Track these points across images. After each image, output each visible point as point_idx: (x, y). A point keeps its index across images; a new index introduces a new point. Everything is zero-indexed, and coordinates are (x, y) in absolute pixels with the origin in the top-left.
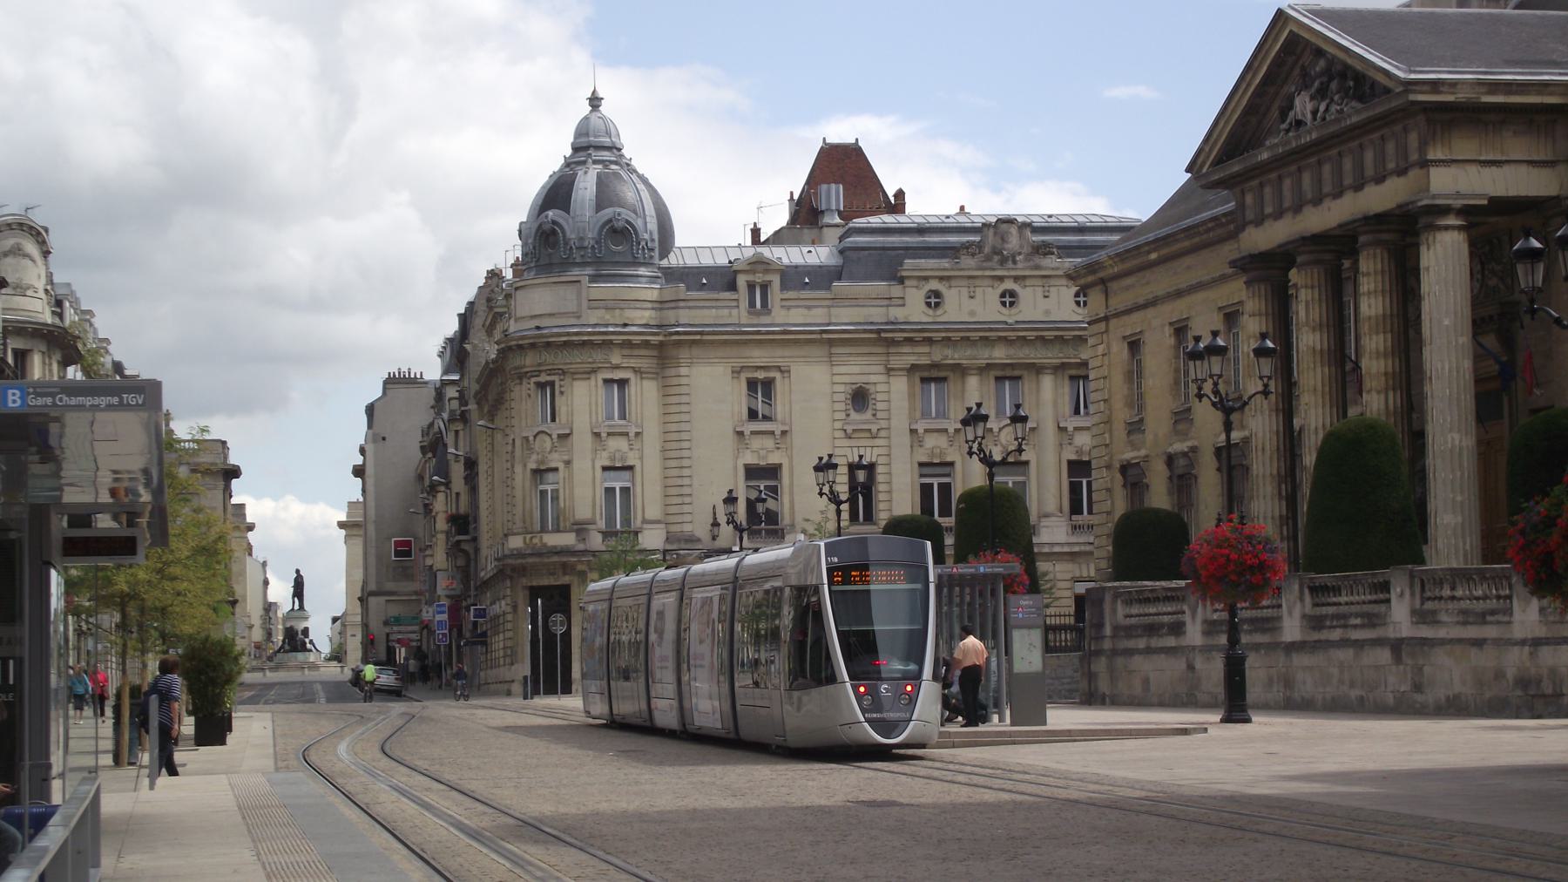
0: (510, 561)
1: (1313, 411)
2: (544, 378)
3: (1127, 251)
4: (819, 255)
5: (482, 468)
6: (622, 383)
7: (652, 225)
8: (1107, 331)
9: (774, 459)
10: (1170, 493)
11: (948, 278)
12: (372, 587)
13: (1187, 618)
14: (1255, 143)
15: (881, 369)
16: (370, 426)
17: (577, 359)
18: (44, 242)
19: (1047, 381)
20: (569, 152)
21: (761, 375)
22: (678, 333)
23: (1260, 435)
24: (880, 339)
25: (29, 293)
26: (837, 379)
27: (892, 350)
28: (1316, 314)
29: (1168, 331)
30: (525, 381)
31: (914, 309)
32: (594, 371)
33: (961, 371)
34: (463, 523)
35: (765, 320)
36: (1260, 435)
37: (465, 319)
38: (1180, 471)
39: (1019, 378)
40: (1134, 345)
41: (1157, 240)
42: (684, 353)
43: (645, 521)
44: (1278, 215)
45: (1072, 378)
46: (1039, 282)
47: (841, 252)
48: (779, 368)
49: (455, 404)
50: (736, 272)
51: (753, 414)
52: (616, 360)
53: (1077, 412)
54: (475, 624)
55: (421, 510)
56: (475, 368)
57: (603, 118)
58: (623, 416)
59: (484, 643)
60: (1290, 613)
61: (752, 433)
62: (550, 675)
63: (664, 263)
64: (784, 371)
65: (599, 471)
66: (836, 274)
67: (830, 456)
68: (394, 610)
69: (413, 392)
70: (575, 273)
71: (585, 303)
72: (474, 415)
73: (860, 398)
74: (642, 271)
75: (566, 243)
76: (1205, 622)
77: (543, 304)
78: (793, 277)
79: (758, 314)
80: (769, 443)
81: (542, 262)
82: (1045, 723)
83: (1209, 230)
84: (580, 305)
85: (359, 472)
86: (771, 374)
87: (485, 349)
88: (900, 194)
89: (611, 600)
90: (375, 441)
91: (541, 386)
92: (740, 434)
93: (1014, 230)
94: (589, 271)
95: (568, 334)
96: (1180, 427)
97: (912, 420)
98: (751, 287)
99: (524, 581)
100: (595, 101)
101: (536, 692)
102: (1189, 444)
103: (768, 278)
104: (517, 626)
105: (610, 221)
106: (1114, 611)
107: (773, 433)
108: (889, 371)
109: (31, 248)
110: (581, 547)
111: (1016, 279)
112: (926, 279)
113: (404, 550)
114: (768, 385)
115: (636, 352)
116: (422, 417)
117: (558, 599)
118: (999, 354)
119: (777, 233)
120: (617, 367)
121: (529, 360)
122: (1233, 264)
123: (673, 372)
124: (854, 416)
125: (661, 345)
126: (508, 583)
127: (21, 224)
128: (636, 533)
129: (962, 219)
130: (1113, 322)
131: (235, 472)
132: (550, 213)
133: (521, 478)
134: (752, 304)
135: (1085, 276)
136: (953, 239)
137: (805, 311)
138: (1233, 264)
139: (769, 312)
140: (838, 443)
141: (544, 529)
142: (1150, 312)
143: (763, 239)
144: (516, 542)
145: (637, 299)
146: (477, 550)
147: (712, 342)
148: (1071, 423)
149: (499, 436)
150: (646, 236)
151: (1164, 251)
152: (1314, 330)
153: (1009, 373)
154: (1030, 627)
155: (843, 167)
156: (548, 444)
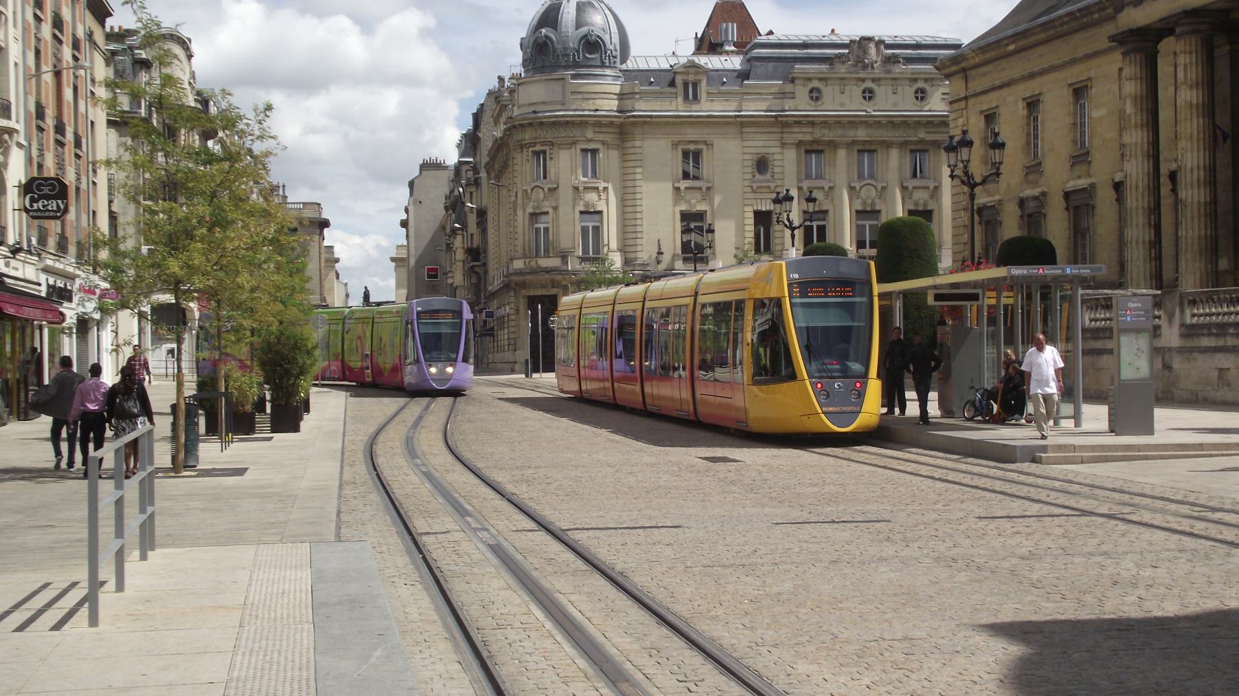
0: (514, 278)
1: (1189, 154)
2: (538, 148)
3: (989, 45)
5: (490, 215)
6: (594, 152)
7: (616, 39)
8: (966, 108)
9: (701, 207)
13: (1163, 323)
15: (778, 143)
16: (411, 194)
19: (894, 154)
21: (692, 147)
22: (634, 116)
23: (1134, 175)
24: (777, 122)
26: (746, 150)
27: (785, 130)
28: (1193, 74)
29: (1021, 104)
31: (800, 105)
32: (575, 143)
33: (834, 145)
34: (475, 254)
35: (694, 107)
36: (1134, 175)
37: (477, 118)
38: (1030, 211)
39: (874, 151)
40: (1032, 104)
41: (1012, 36)
42: (638, 130)
45: (911, 151)
46: (890, 82)
48: (705, 143)
49: (470, 174)
50: (675, 73)
52: (590, 135)
53: (915, 176)
54: (485, 322)
55: (444, 248)
56: (486, 144)
59: (493, 335)
62: (543, 359)
63: (624, 67)
64: (709, 145)
66: (743, 75)
67: (965, 132)
69: (439, 173)
72: (484, 182)
73: (762, 165)
74: (608, 72)
75: (554, 51)
76: (1182, 325)
77: (537, 93)
80: (698, 195)
82: (1150, 431)
83: (1066, 23)
84: (564, 95)
85: (404, 224)
86: (700, 147)
87: (492, 133)
89: (696, 293)
93: (872, 45)
95: (556, 116)
96: (1031, 177)
97: (800, 181)
98: (686, 84)
99: (525, 292)
101: (536, 370)
102: (1040, 190)
104: (519, 326)
105: (585, 36)
109: (178, 50)
111: (874, 80)
112: (810, 79)
113: (433, 274)
114: (697, 155)
115: (604, 130)
116: (444, 189)
117: (551, 304)
118: (861, 134)
120: (590, 140)
121: (528, 136)
122: (1112, 38)
123: (630, 144)
124: (758, 176)
126: (512, 293)
129: (834, 38)
130: (972, 101)
131: (325, 224)
132: (544, 31)
133: (521, 218)
134: (686, 97)
135: (950, 66)
138: (1112, 38)
140: (746, 196)
141: (537, 256)
142: (1005, 91)
144: (518, 264)
145: (603, 93)
146: (486, 272)
147: (658, 123)
148: (911, 184)
149: (504, 192)
150: (611, 47)
151: (1021, 43)
152: (1191, 87)
153: (867, 147)
156: (541, 196)
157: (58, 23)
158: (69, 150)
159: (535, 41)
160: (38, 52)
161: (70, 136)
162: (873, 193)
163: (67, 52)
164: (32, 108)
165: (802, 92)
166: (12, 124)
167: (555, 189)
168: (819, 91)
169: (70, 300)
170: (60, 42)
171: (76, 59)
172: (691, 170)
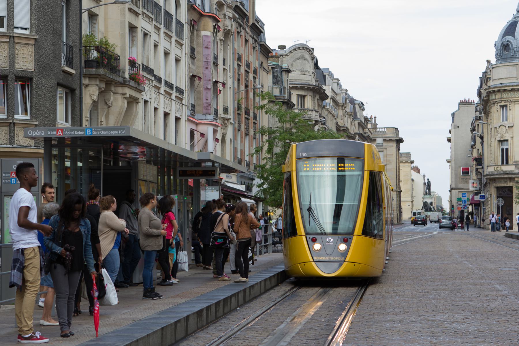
2: (503, 104)
5: (485, 139)
12: (453, 186)
16: (453, 122)
18: (312, 54)
25: (306, 73)
30: (496, 105)
68: (460, 195)
81: (503, 57)
85: (449, 140)
90: (454, 128)
91: (502, 107)
121: (497, 96)
127: (303, 47)
156: (504, 130)
157: (248, 65)
158: (251, 120)
159: (503, 43)
160: (239, 80)
161: (251, 114)
163: (251, 76)
164: (236, 106)
166: (228, 116)
167: (512, 126)
169: (426, 202)
170: (249, 72)
171: (255, 78)
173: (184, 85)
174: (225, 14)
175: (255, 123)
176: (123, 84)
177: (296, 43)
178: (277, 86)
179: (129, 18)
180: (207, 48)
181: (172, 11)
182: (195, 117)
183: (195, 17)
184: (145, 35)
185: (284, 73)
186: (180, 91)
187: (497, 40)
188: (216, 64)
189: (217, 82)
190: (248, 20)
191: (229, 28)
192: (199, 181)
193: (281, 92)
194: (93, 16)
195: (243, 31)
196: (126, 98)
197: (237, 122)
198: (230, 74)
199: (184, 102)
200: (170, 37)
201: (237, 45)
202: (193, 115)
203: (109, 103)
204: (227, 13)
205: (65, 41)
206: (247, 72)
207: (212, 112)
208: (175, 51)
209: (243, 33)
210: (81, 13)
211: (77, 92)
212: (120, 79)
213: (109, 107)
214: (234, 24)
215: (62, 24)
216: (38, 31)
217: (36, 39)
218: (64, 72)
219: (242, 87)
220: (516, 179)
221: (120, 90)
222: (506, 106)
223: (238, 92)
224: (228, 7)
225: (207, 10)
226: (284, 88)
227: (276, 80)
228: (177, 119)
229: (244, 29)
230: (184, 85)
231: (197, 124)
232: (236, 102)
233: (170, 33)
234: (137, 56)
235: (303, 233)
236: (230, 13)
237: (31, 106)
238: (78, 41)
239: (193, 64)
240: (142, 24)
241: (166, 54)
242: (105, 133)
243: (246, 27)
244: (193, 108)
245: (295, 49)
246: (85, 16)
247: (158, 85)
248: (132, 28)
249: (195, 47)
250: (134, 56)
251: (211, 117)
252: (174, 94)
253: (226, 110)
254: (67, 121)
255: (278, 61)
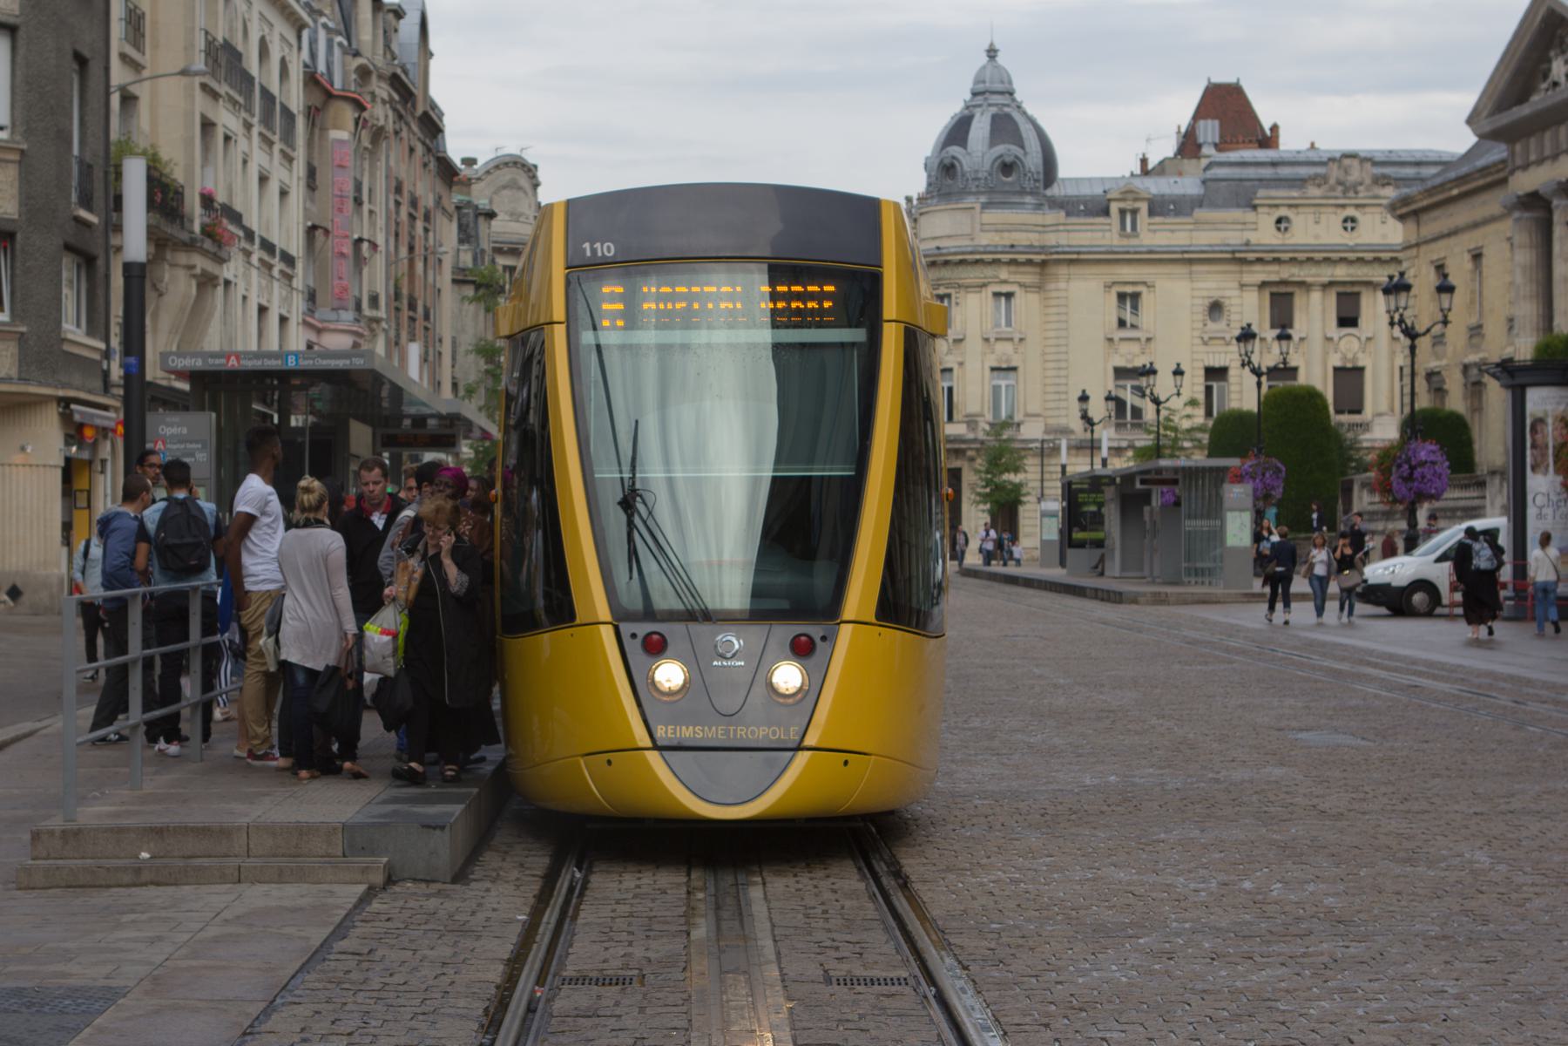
4: (1188, 185)
10: (1465, 398)
11: (1296, 206)
14: (1522, 98)
15: (1236, 285)
17: (971, 275)
20: (968, 96)
21: (1129, 289)
26: (1196, 293)
29: (1467, 257)
31: (1264, 233)
32: (984, 285)
35: (1134, 242)
38: (1473, 379)
42: (1063, 270)
43: (1027, 415)
44: (1540, 161)
47: (1204, 182)
48: (1144, 283)
51: (1122, 323)
57: (998, 67)
58: (1009, 323)
60: (1492, 504)
61: (1122, 339)
65: (987, 372)
66: (1198, 202)
70: (970, 201)
71: (978, 227)
74: (1028, 199)
78: (1158, 207)
79: (1128, 236)
80: (1134, 348)
88: (1275, 128)
92: (1110, 340)
94: (983, 199)
96: (1475, 340)
98: (1122, 212)
100: (992, 53)
102: (1481, 355)
103: (1137, 205)
106: (1361, 498)
107: (1138, 339)
108: (1242, 286)
109: (524, 182)
110: (971, 436)
111: (1357, 206)
112: (1277, 206)
114: (1135, 297)
119: (1161, 163)
120: (1005, 282)
123: (1052, 286)
124: (1211, 326)
125: (1044, 264)
128: (1019, 425)
130: (1423, 249)
136: (1303, 171)
137: (1169, 235)
139: (1137, 236)
142: (1452, 240)
143: (1150, 166)
154: (1242, 510)
155: (1226, 107)
157: (414, 203)
160: (397, 235)
161: (420, 309)
162: (1355, 345)
163: (420, 225)
164: (392, 291)
165: (1266, 220)
167: (961, 340)
168: (1287, 219)
171: (426, 230)
172: (1128, 318)
173: (296, 247)
174: (373, 94)
175: (426, 329)
176: (190, 246)
177: (500, 153)
178: (465, 247)
179: (201, 103)
180: (341, 166)
181: (275, 88)
182: (317, 315)
183: (317, 99)
184: (227, 138)
185: (481, 219)
186: (288, 259)
187: (929, 154)
188: (358, 202)
189: (360, 240)
190: (414, 106)
191: (382, 122)
192: (400, 456)
193: (475, 259)
194: (128, 99)
195: (405, 129)
196: (194, 276)
197: (393, 325)
198: (381, 221)
199: (295, 283)
200: (270, 143)
201: (396, 159)
202: (311, 312)
203: (162, 287)
204: (378, 91)
205: (76, 151)
206: (412, 217)
207: (352, 304)
208: (278, 174)
209: (404, 134)
210: (108, 94)
211: (100, 262)
212: (184, 236)
213: (161, 295)
214: (390, 113)
215: (71, 118)
216: (29, 133)
217: (22, 152)
218: (78, 220)
219: (404, 252)
220: (969, 453)
221: (182, 258)
222: (949, 296)
223: (396, 262)
224: (380, 77)
225: (338, 84)
226: (483, 251)
227: (466, 235)
228: (283, 320)
229: (407, 124)
230: (296, 247)
231: (319, 331)
232: (392, 283)
233: (269, 134)
234: (216, 183)
235: (603, 611)
236: (383, 90)
237: (13, 294)
238: (102, 154)
239: (313, 200)
240: (227, 119)
241: (263, 179)
242: (325, 362)
243: (409, 119)
244: (312, 297)
245: (497, 167)
246: (115, 100)
247: (248, 246)
248: (207, 126)
249: (316, 163)
250: (210, 185)
251: (348, 316)
252: (278, 266)
253: (374, 301)
254: (78, 325)
255: (469, 194)
